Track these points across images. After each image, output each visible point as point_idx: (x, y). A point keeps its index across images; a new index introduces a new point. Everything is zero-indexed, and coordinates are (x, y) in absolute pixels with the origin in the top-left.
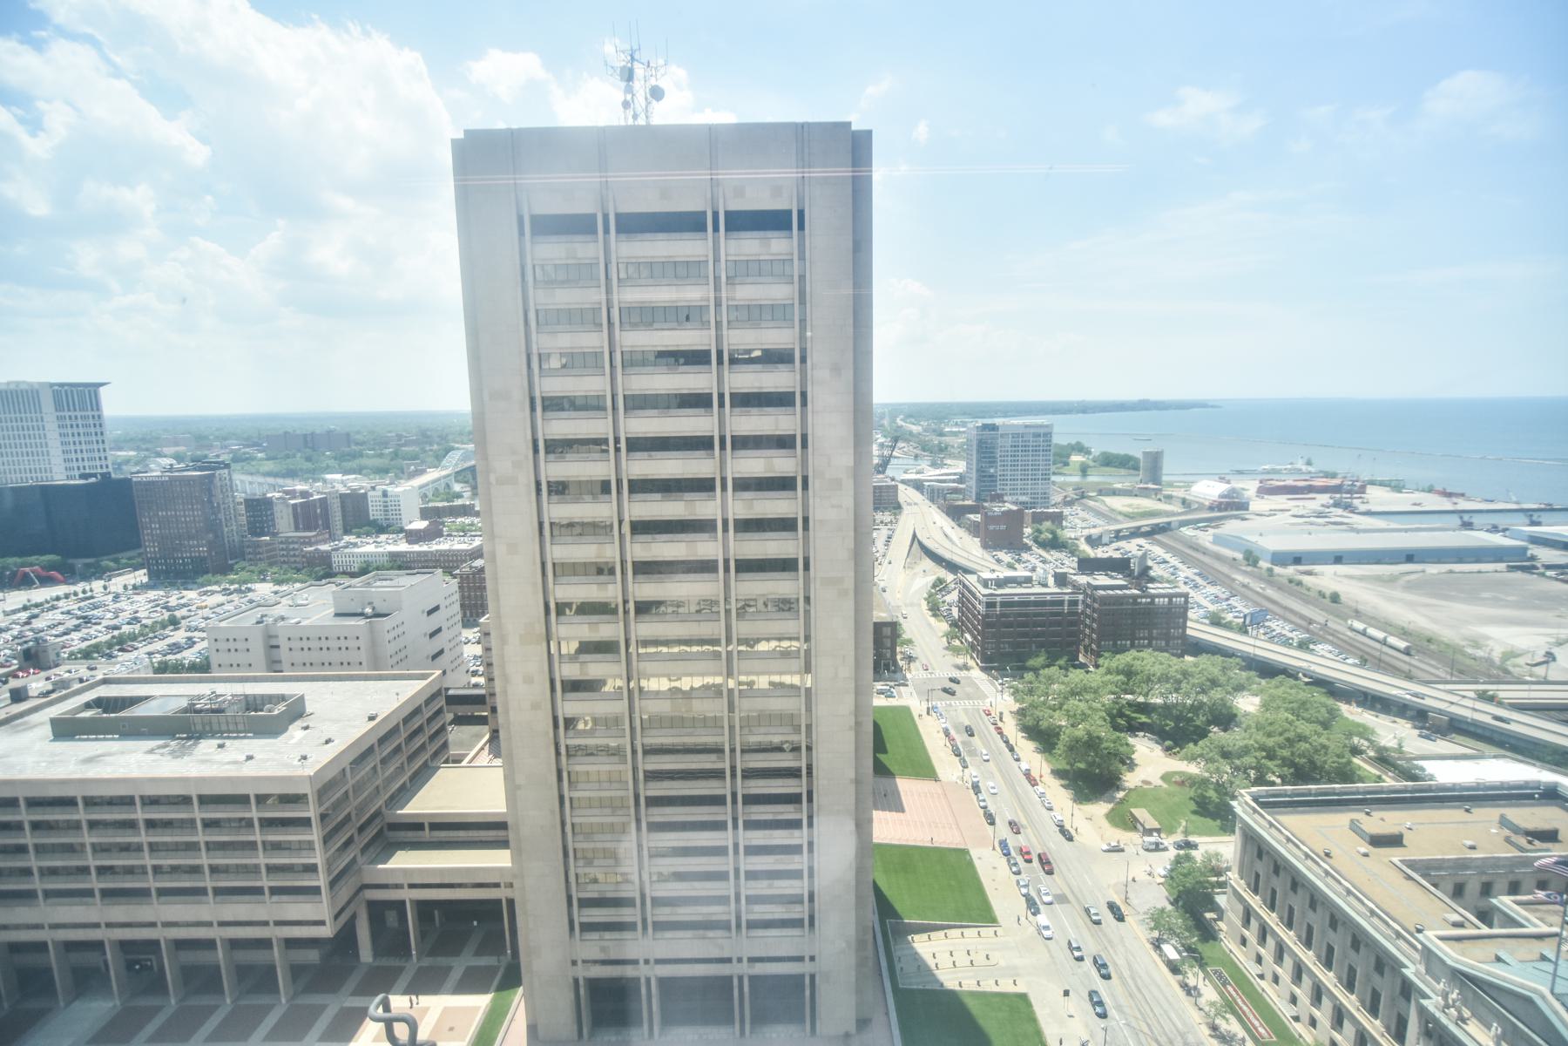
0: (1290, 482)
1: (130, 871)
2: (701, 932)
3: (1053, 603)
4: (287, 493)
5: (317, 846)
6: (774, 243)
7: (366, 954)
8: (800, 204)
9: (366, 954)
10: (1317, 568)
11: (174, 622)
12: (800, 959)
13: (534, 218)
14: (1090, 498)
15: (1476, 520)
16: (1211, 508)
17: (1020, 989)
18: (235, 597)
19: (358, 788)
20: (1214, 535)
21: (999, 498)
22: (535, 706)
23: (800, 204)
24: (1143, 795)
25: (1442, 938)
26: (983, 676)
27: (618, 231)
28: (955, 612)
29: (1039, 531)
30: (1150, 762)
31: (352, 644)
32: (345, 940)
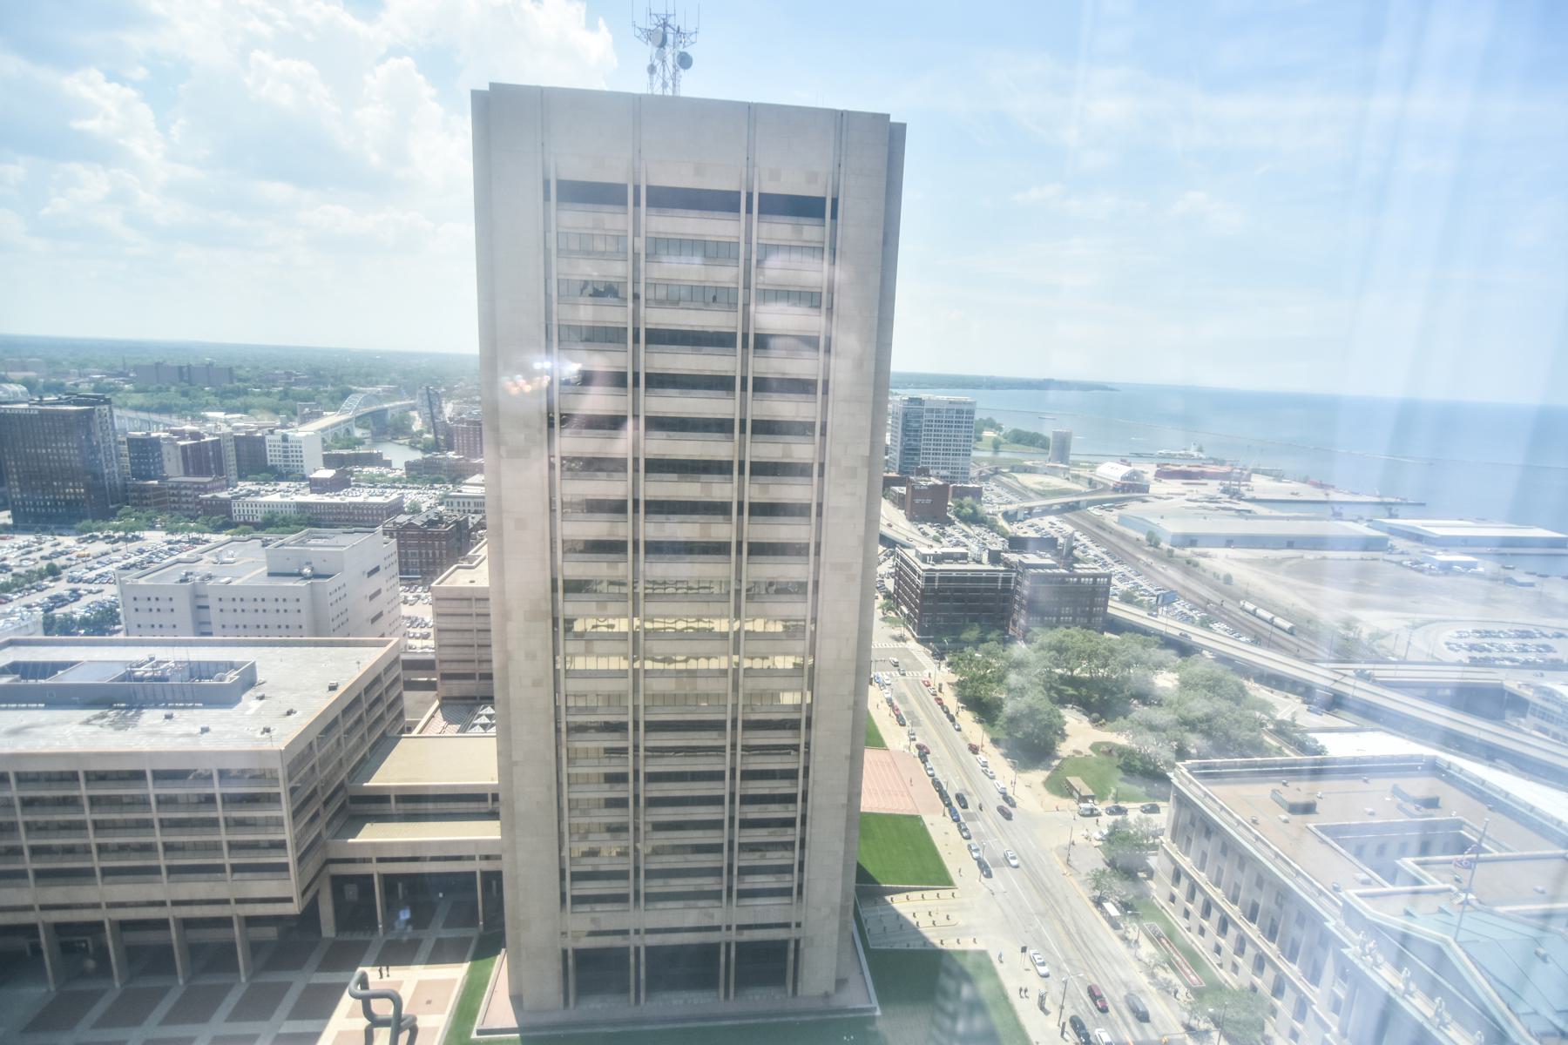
0: (1184, 468)
1: (70, 850)
2: (692, 903)
3: (987, 580)
4: (174, 433)
5: (286, 822)
6: (806, 229)
7: (328, 929)
8: (836, 190)
9: (328, 929)
10: (1211, 551)
11: (54, 572)
12: (786, 925)
13: (560, 183)
14: (1003, 474)
15: (1346, 511)
16: (1115, 490)
17: (980, 946)
18: (121, 545)
19: (324, 762)
20: (1121, 517)
21: (924, 472)
22: (537, 684)
23: (838, 192)
24: (1077, 763)
25: (1360, 896)
26: (920, 648)
27: (649, 205)
28: (890, 585)
29: (961, 506)
30: (1080, 734)
31: (291, 606)
32: (310, 914)
